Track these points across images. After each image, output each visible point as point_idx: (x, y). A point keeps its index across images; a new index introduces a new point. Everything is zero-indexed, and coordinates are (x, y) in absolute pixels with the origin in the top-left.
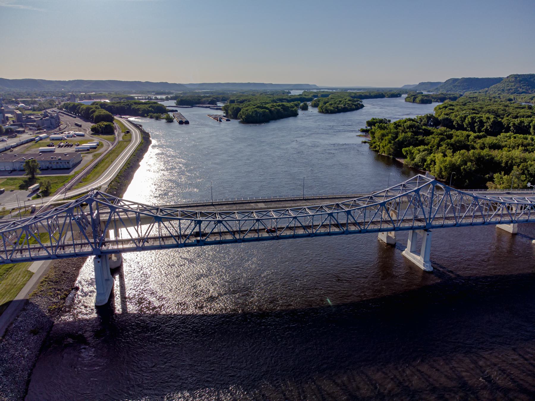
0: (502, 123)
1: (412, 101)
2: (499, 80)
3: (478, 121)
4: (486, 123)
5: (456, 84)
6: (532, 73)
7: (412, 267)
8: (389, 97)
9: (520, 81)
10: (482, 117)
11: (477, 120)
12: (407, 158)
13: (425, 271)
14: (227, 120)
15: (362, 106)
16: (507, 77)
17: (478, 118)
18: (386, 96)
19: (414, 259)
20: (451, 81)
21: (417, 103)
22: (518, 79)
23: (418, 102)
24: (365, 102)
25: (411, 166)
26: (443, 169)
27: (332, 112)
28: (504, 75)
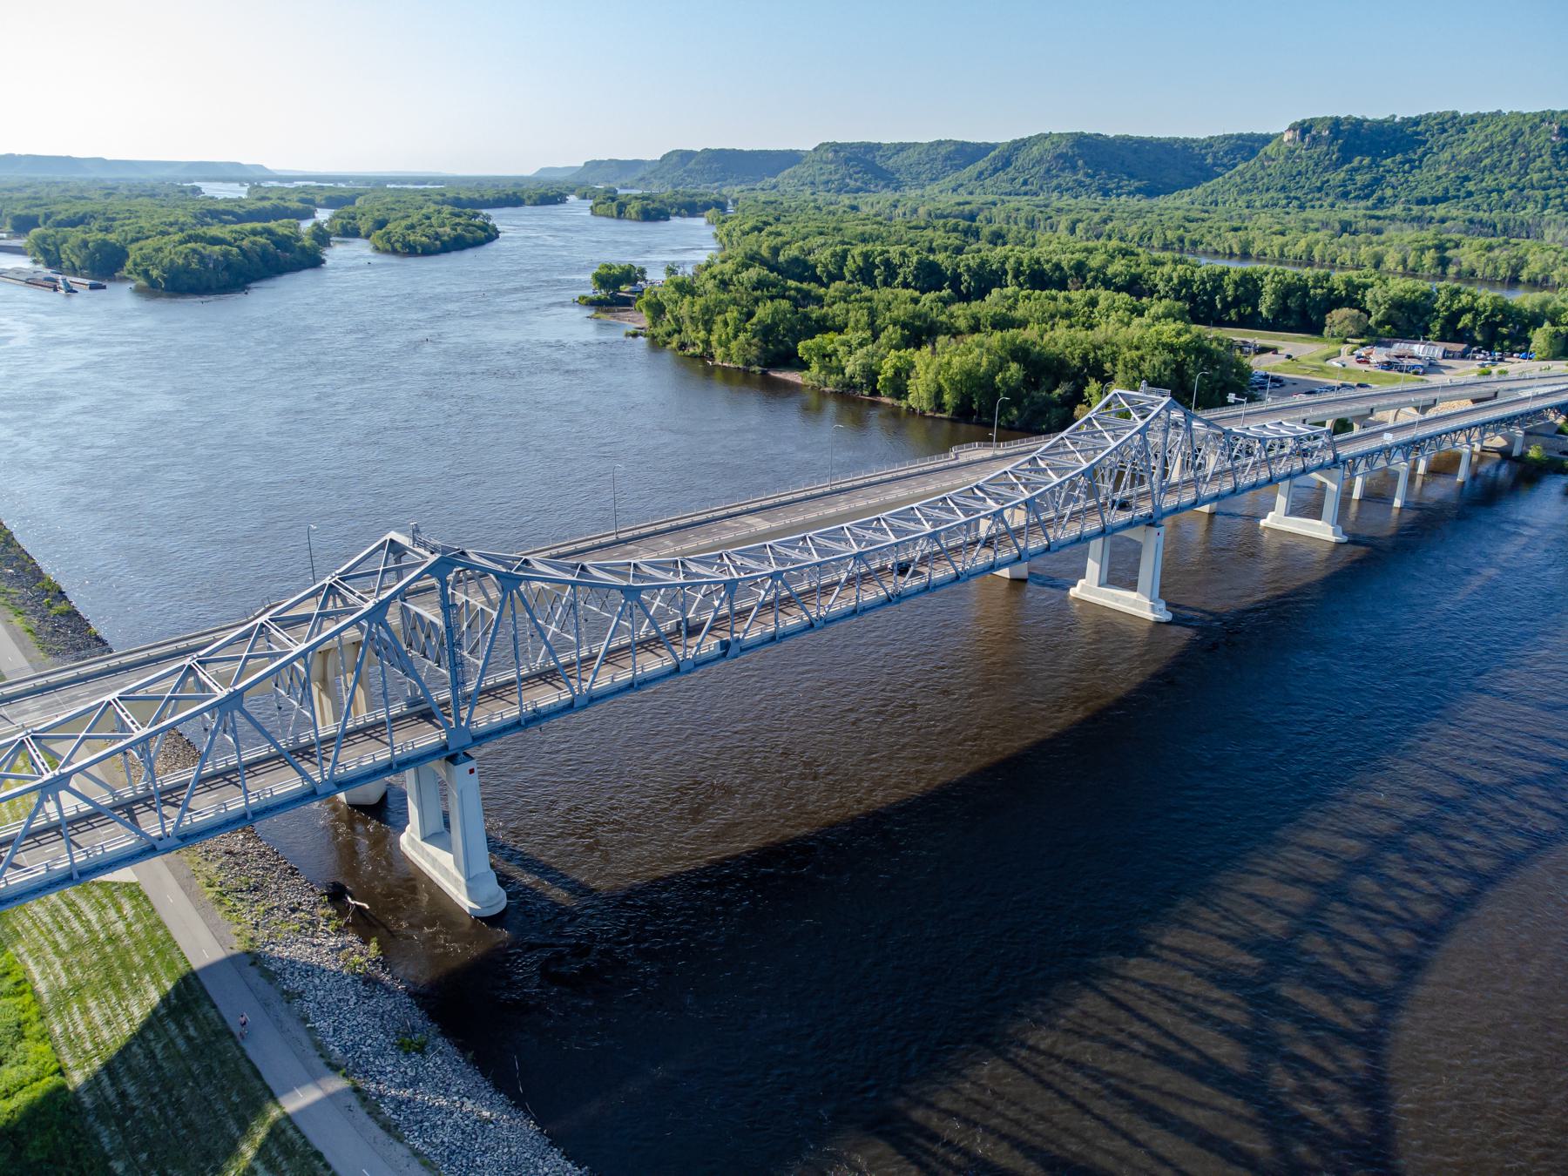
0: (939, 266)
1: (615, 213)
2: (791, 158)
3: (881, 261)
4: (901, 266)
5: (691, 165)
6: (866, 140)
7: (1109, 625)
8: (535, 204)
9: (847, 161)
10: (888, 252)
11: (877, 261)
12: (808, 368)
13: (1158, 623)
14: (92, 287)
15: (491, 235)
16: (815, 149)
17: (880, 255)
18: (528, 202)
19: (1117, 600)
20: (675, 159)
21: (630, 219)
22: (842, 154)
23: (634, 215)
24: (499, 218)
25: (832, 389)
26: (946, 386)
27: (427, 252)
28: (805, 143)
